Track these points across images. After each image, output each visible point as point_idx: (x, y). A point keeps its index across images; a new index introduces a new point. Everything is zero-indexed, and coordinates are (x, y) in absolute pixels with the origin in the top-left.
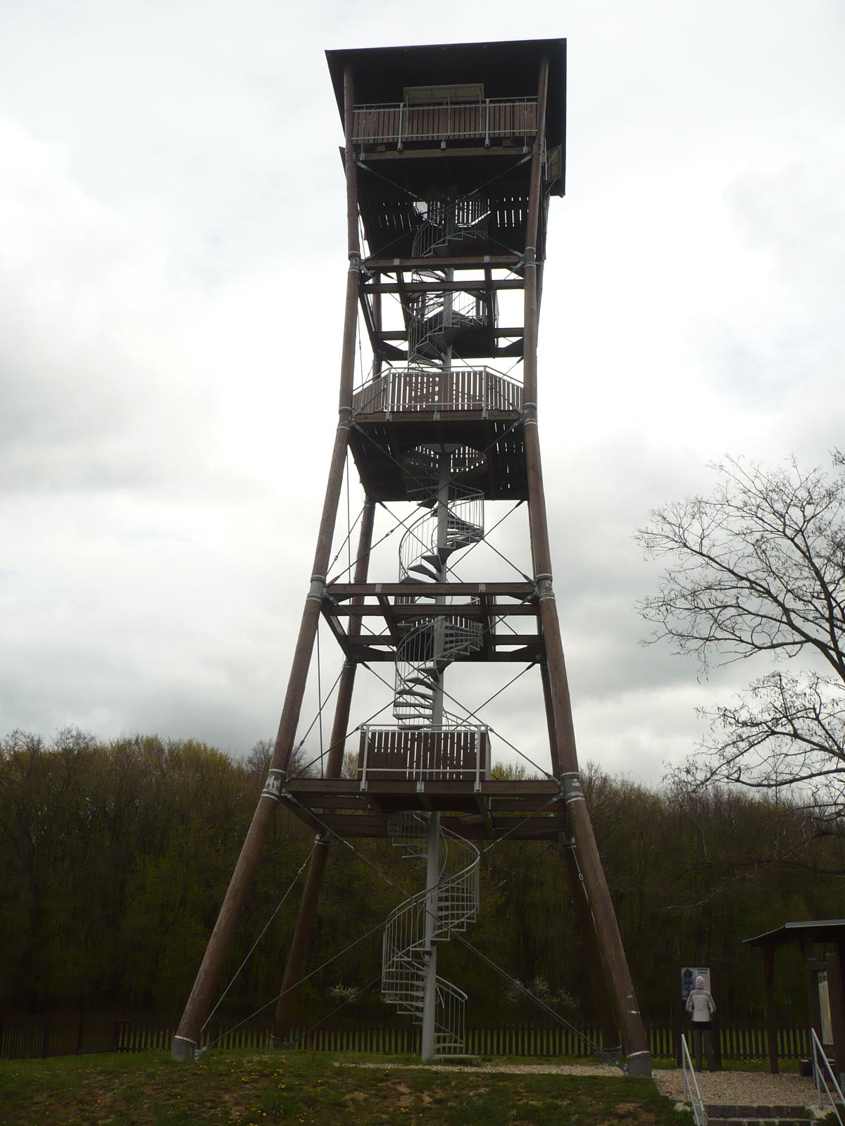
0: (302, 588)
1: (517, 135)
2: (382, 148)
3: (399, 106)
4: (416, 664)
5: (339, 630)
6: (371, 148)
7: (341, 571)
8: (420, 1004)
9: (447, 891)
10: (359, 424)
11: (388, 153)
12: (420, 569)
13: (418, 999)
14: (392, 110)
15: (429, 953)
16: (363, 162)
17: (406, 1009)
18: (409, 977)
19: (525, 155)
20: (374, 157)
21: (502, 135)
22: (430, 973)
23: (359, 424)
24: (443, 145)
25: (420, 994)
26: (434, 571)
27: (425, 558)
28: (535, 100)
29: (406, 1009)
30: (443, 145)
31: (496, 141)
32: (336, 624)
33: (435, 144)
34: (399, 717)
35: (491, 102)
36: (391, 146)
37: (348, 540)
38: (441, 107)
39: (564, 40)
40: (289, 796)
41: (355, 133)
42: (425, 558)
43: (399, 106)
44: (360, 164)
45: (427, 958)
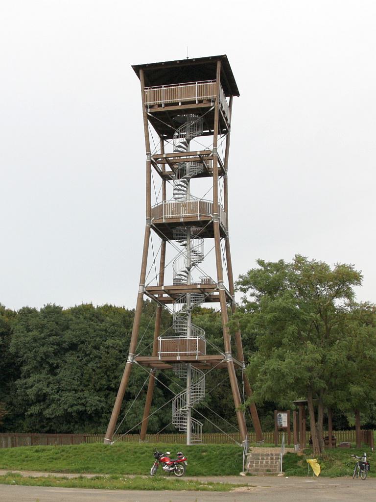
0: (144, 159)
1: (208, 98)
2: (157, 106)
3: (162, 87)
4: (181, 180)
5: (159, 170)
6: (151, 107)
7: (152, 281)
8: (185, 332)
9: (194, 389)
10: (154, 224)
11: (159, 108)
12: (180, 146)
13: (185, 330)
14: (159, 89)
15: (187, 411)
16: (150, 113)
17: (182, 429)
18: (182, 419)
19: (212, 107)
20: (154, 110)
21: (202, 99)
22: (189, 419)
23: (154, 224)
24: (180, 104)
25: (185, 424)
26: (185, 147)
27: (181, 143)
28: (215, 81)
29: (182, 429)
30: (180, 104)
31: (200, 102)
32: (157, 168)
33: (177, 104)
34: (176, 199)
35: (198, 83)
36: (160, 106)
37: (154, 264)
38: (178, 87)
39: (226, 55)
40: (136, 362)
41: (146, 101)
42: (181, 143)
43: (162, 87)
44: (149, 114)
45: (188, 412)
